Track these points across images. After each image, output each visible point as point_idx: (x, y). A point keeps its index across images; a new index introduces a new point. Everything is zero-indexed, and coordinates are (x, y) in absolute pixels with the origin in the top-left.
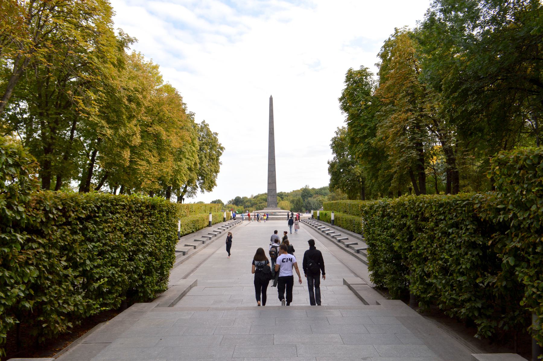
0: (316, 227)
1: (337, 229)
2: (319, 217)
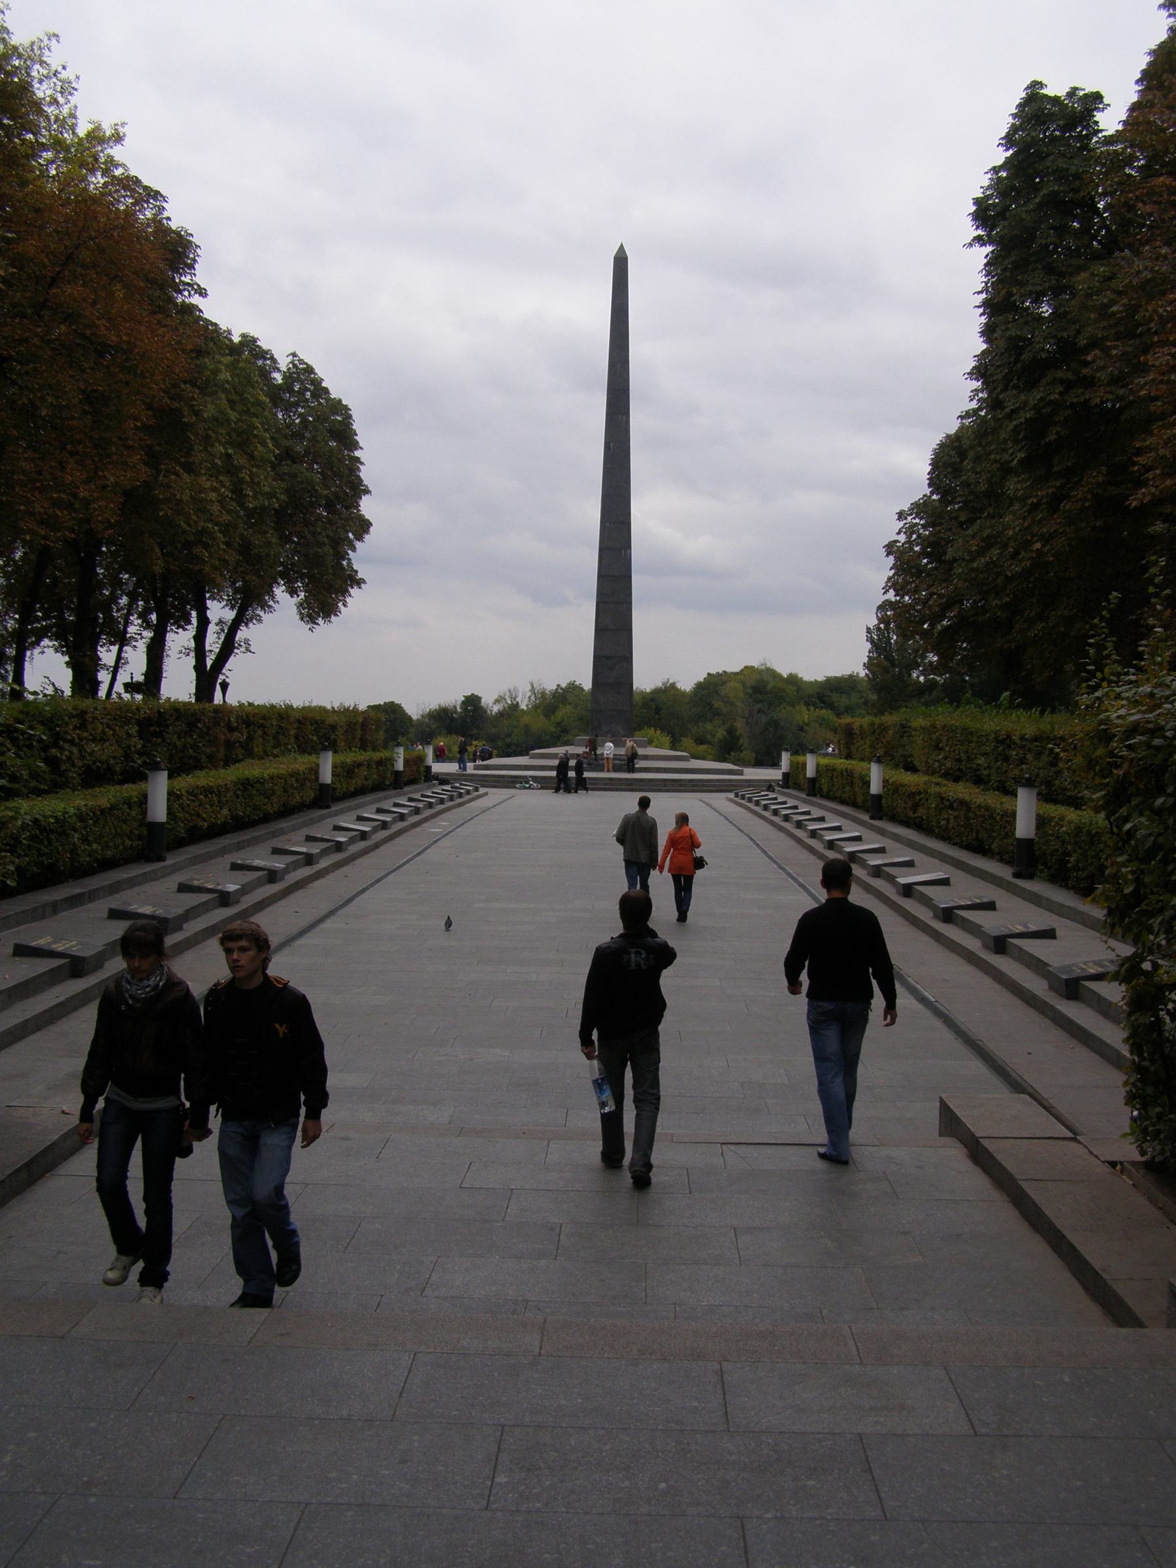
0: (799, 825)
1: (896, 838)
2: (813, 781)
